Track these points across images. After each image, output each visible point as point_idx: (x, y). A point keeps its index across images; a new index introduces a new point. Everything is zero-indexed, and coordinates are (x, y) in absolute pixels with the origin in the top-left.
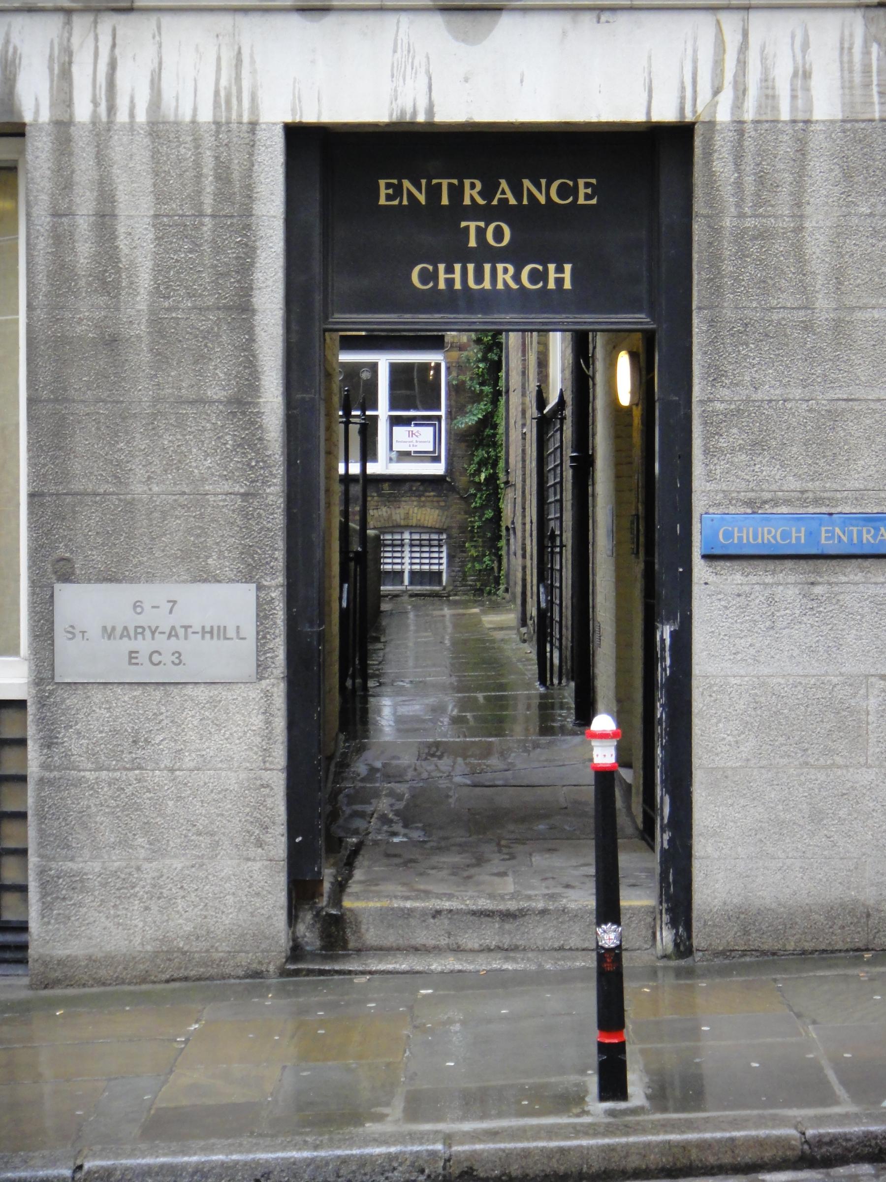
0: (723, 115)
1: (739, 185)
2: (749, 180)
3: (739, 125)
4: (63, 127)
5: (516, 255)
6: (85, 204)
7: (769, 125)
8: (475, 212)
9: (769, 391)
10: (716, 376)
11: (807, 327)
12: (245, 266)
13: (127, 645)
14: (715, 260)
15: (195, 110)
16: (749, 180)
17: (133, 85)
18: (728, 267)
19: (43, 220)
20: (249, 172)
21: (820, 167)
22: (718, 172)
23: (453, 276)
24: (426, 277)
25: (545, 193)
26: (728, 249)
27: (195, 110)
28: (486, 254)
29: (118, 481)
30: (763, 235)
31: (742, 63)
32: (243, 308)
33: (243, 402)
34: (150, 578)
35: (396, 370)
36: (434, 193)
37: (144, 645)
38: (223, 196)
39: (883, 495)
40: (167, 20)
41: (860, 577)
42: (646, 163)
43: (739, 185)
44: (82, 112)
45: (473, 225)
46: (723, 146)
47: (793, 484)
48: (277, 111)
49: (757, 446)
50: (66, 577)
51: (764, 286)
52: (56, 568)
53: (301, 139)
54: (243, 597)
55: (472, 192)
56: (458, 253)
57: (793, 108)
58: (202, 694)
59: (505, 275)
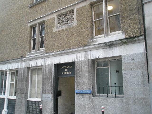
0: (77, 61)
1: (78, 65)
2: (78, 65)
3: (44, 65)
4: (44, 65)
5: (68, 71)
6: (45, 70)
7: (79, 61)
8: (66, 69)
9: (80, 81)
10: (77, 80)
11: (82, 76)
12: (52, 73)
13: (46, 98)
14: (76, 71)
15: (42, 64)
16: (78, 65)
17: (47, 62)
18: (77, 72)
19: (43, 71)
20: (52, 67)
21: (83, 64)
22: (77, 64)
23: (64, 73)
24: (63, 73)
25: (69, 67)
26: (77, 70)
27: (42, 64)
28: (66, 71)
29: (46, 87)
30: (79, 69)
31: (78, 57)
32: (52, 76)
33: (51, 82)
34: (47, 94)
35: (109, 68)
36: (63, 67)
37: (46, 98)
38: (51, 69)
39: (32, 113)
40: (49, 58)
41: (86, 95)
42: (73, 64)
43: (78, 65)
44: (45, 64)
45: (65, 70)
46: (77, 63)
47: (81, 88)
48: (54, 63)
49: (79, 85)
50: (43, 94)
51: (79, 73)
52: (43, 93)
53: (55, 65)
54: (51, 95)
55: (65, 67)
56: (65, 71)
57: (22, 64)
58: (49, 102)
59: (67, 73)
